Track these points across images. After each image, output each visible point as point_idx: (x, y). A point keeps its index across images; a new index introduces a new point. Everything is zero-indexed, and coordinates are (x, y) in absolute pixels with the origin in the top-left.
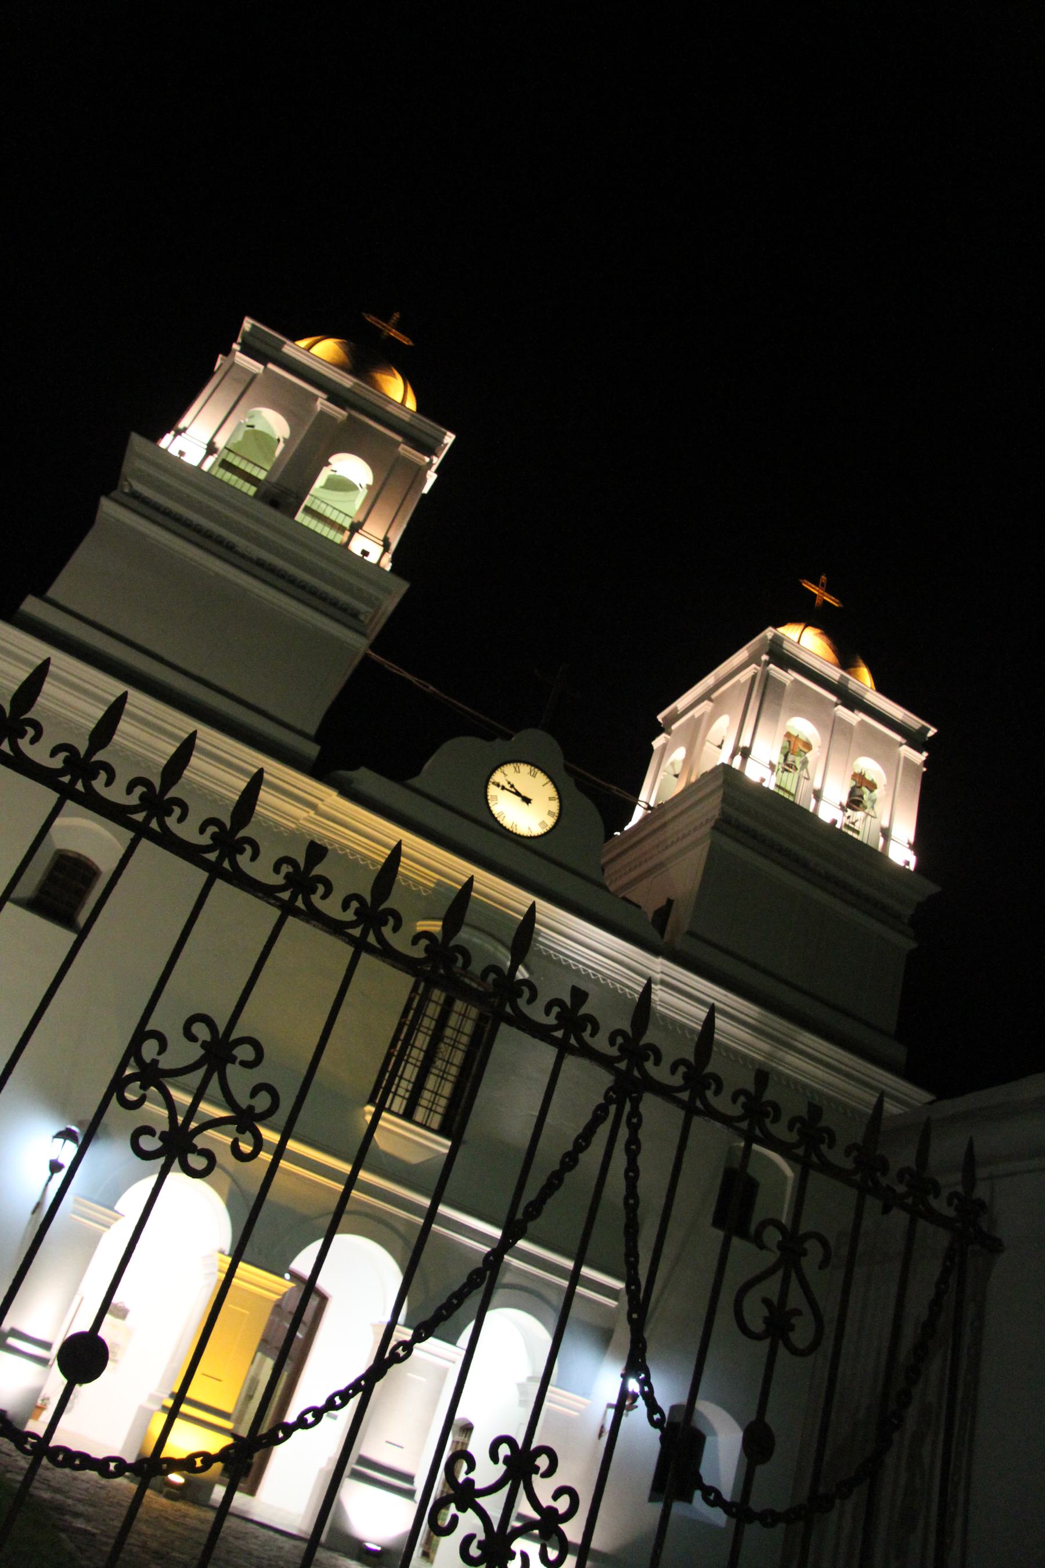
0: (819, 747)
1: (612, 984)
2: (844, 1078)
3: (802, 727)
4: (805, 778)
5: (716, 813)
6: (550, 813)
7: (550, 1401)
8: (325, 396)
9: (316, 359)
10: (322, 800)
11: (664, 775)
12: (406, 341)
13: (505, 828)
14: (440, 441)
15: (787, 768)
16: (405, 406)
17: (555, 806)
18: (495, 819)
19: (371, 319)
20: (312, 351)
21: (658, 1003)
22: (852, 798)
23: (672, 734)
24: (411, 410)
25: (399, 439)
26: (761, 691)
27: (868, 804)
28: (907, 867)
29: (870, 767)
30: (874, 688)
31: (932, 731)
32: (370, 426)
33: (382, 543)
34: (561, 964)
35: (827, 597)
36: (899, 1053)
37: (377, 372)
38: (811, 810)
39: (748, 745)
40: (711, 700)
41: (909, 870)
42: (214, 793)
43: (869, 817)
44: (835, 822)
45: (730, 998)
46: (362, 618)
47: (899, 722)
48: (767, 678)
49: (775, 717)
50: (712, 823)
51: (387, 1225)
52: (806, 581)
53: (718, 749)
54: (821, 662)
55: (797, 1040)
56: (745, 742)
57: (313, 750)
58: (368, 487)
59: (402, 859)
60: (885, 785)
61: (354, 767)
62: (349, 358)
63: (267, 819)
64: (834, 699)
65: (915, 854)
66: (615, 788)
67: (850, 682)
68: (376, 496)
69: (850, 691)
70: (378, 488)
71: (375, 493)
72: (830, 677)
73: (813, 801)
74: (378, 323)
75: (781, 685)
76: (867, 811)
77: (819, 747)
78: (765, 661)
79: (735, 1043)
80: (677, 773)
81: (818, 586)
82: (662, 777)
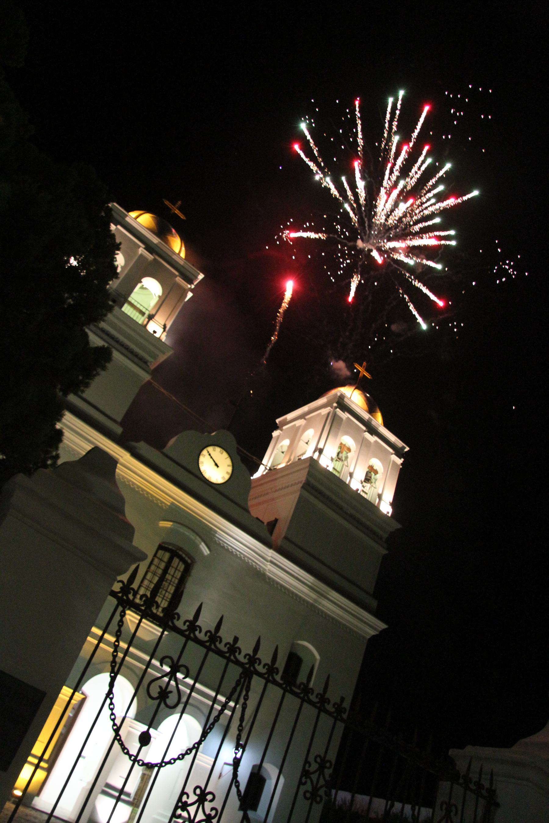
0: (355, 451)
1: (248, 560)
2: (344, 612)
3: (348, 440)
4: (346, 466)
5: (304, 479)
6: (227, 473)
7: (198, 760)
8: (143, 246)
9: (140, 225)
10: (122, 457)
11: (277, 452)
12: (182, 217)
13: (205, 478)
14: (196, 277)
15: (338, 460)
16: (179, 255)
17: (230, 470)
18: (201, 473)
19: (167, 203)
20: (138, 220)
21: (268, 571)
22: (366, 477)
23: (283, 431)
24: (182, 258)
25: (177, 273)
26: (332, 421)
27: (373, 480)
28: (388, 515)
29: (377, 463)
30: (383, 425)
31: (407, 449)
32: (163, 265)
33: (163, 327)
34: (229, 550)
35: (365, 373)
36: (374, 604)
37: (169, 236)
38: (347, 482)
39: (322, 447)
40: (305, 419)
41: (388, 516)
42: (75, 450)
43: (373, 488)
44: (358, 490)
45: (301, 572)
46: (149, 364)
47: (393, 443)
48: (335, 415)
49: (336, 435)
50: (301, 485)
51: (132, 670)
52: (356, 364)
53: (306, 445)
54: (361, 410)
55: (329, 595)
56: (321, 446)
57: (119, 430)
58: (159, 297)
59: (118, 465)
60: (382, 473)
61: (138, 441)
62: (156, 226)
63: (68, 446)
64: (364, 428)
65: (392, 508)
66: (255, 458)
67: (373, 421)
68: (162, 302)
69: (372, 426)
70: (164, 297)
71: (162, 299)
72: (361, 415)
73: (349, 478)
74: (170, 205)
75: (341, 419)
76: (372, 484)
77: (355, 451)
78: (335, 407)
79: (273, 575)
80: (283, 451)
81: (361, 367)
82: (276, 452)
